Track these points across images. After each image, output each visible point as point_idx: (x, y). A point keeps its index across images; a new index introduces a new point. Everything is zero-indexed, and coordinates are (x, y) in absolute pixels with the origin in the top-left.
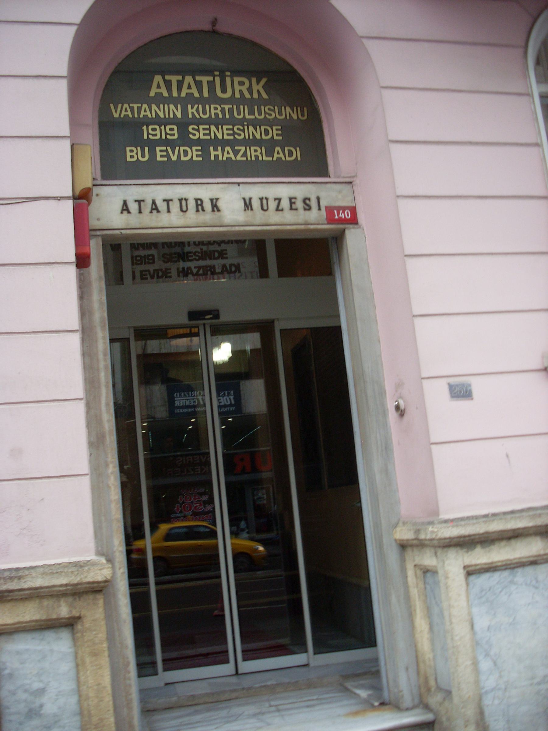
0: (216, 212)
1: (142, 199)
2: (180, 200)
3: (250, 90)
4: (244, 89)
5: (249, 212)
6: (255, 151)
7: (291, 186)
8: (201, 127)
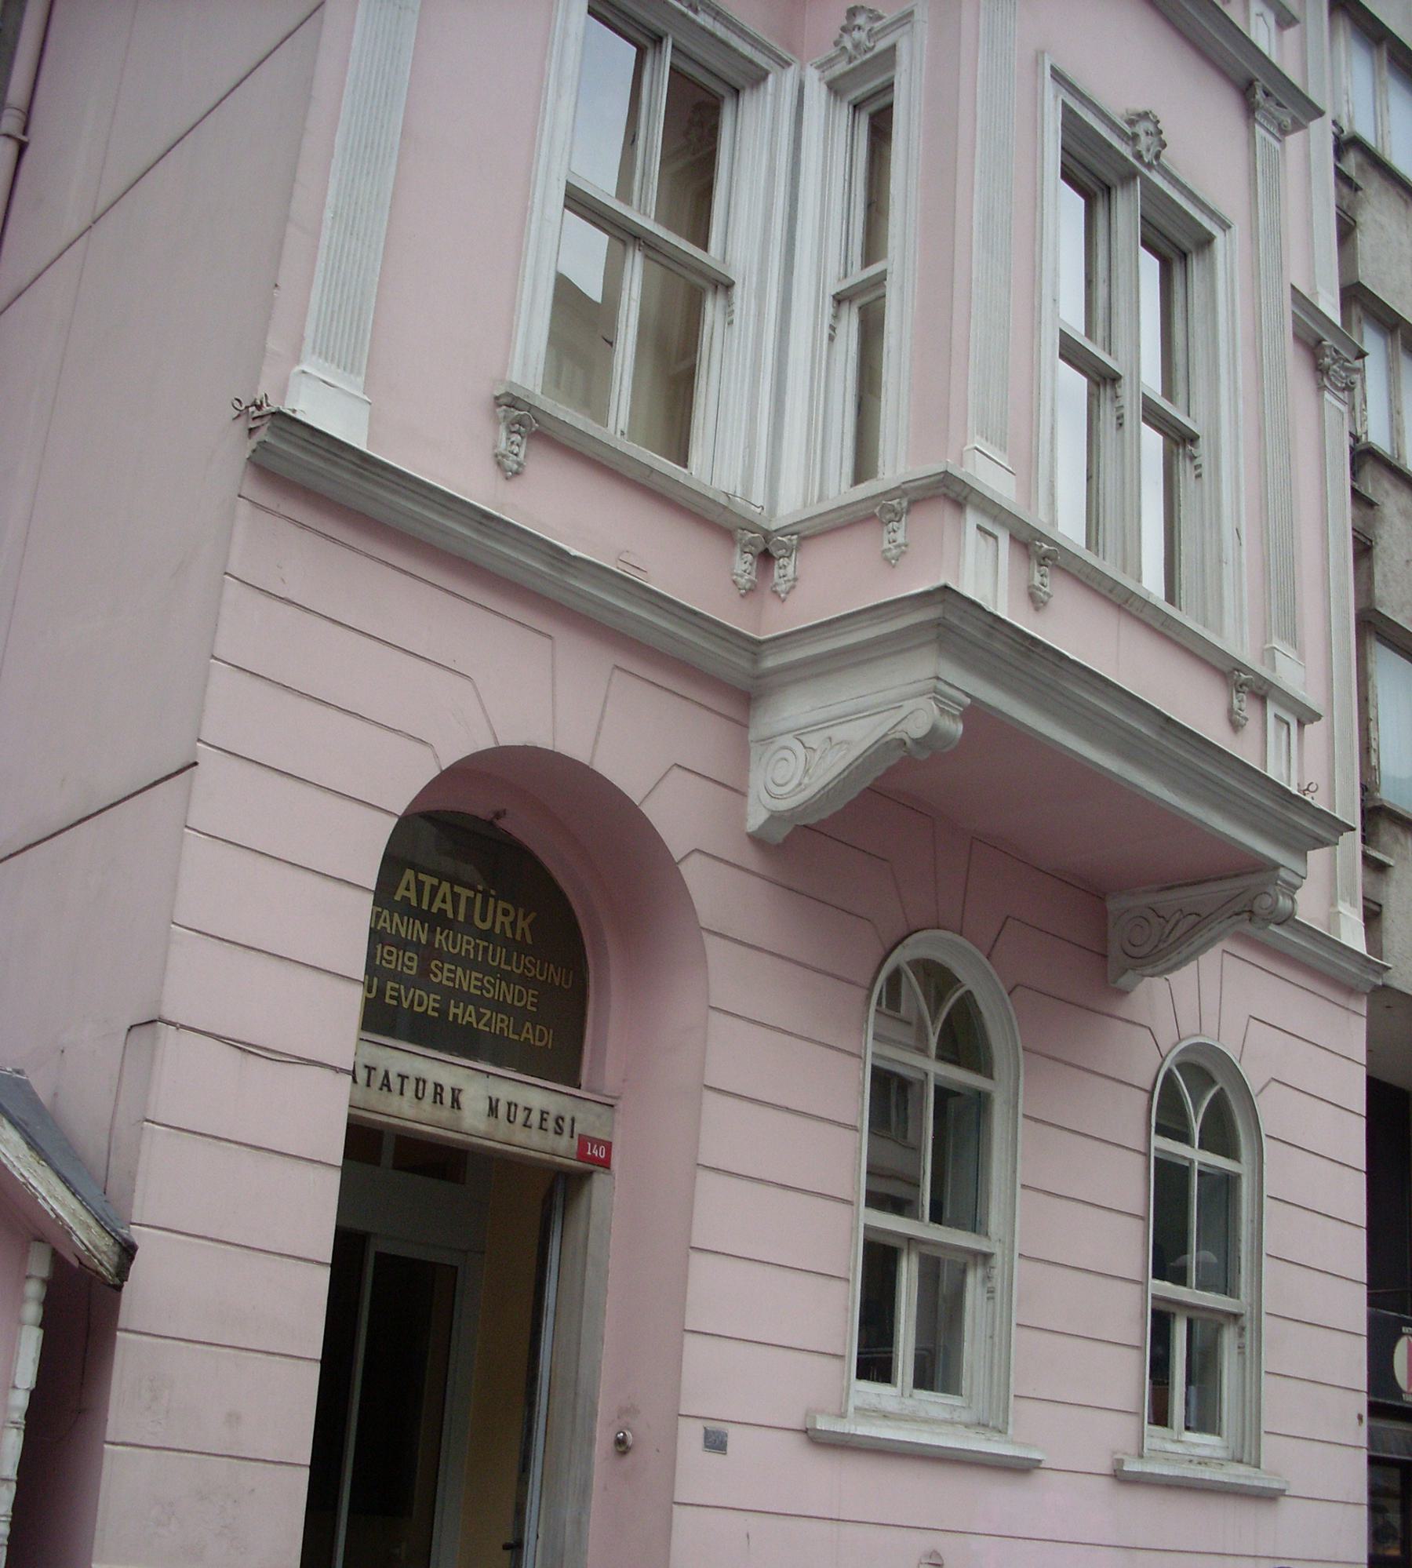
0: (456, 1110)
1: (374, 1066)
2: (418, 1080)
3: (513, 924)
4: (507, 920)
5: (492, 1119)
6: (502, 1021)
7: (546, 1093)
8: (447, 966)
